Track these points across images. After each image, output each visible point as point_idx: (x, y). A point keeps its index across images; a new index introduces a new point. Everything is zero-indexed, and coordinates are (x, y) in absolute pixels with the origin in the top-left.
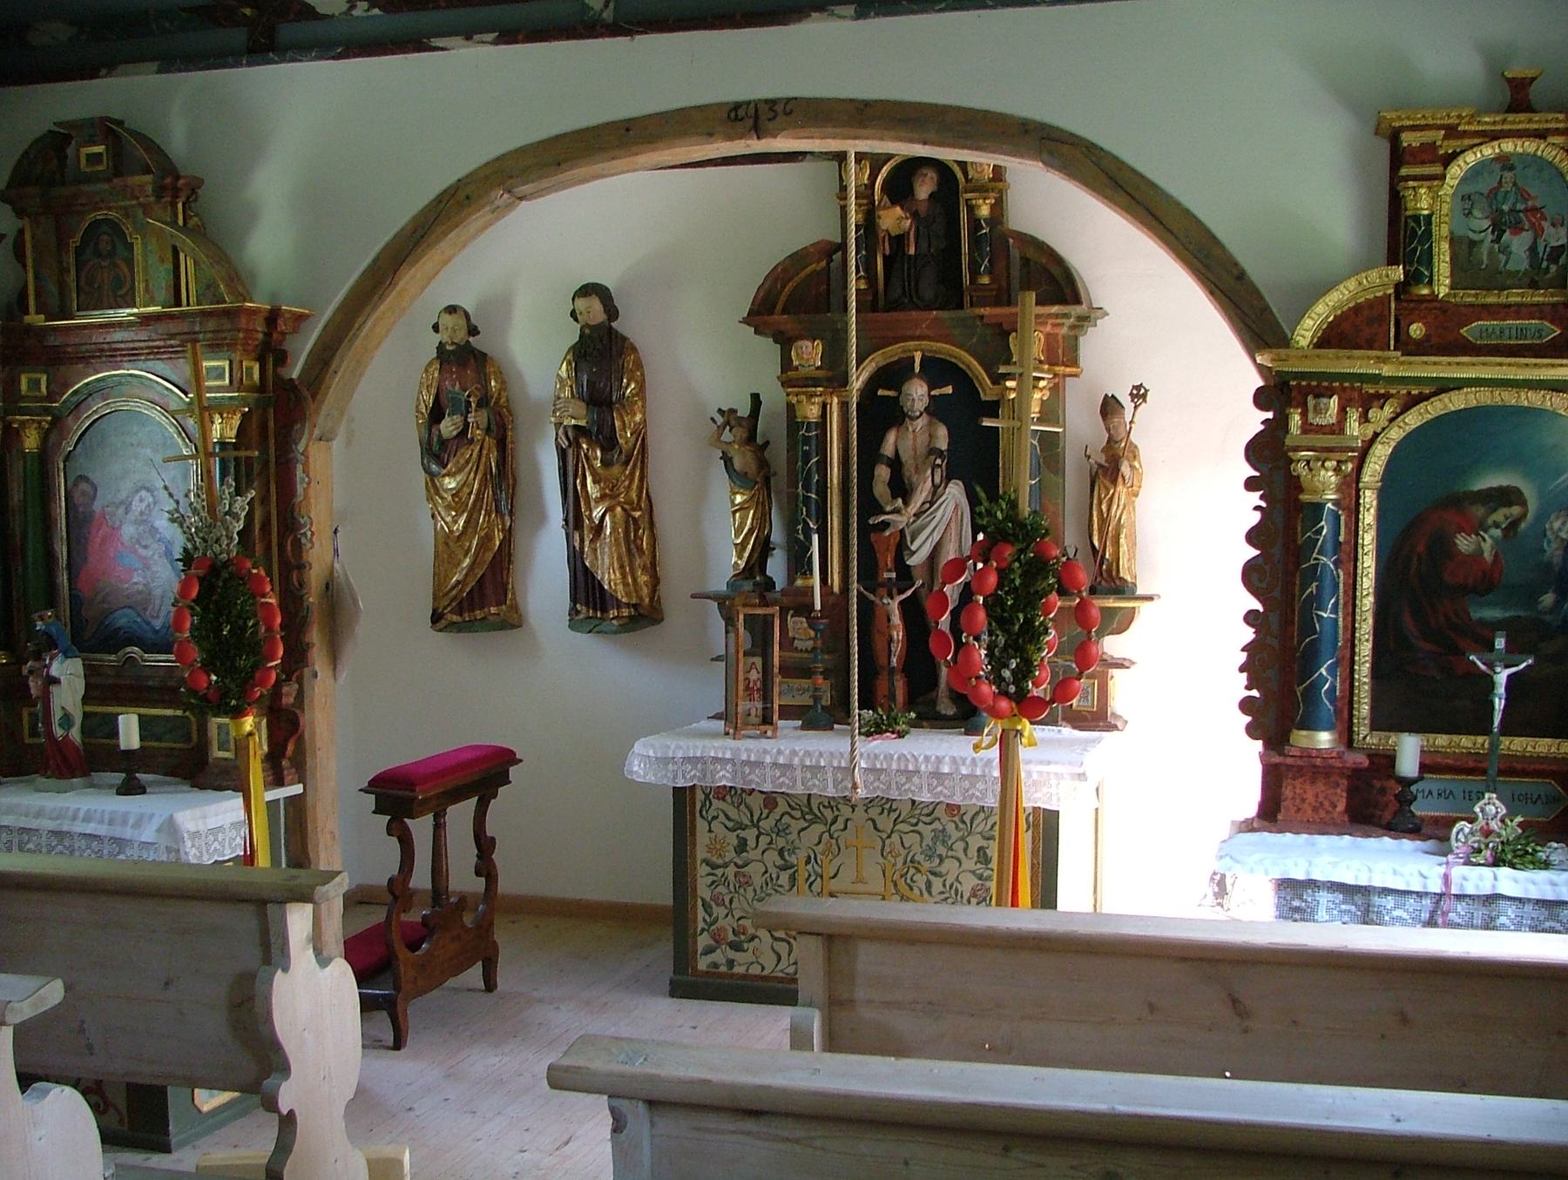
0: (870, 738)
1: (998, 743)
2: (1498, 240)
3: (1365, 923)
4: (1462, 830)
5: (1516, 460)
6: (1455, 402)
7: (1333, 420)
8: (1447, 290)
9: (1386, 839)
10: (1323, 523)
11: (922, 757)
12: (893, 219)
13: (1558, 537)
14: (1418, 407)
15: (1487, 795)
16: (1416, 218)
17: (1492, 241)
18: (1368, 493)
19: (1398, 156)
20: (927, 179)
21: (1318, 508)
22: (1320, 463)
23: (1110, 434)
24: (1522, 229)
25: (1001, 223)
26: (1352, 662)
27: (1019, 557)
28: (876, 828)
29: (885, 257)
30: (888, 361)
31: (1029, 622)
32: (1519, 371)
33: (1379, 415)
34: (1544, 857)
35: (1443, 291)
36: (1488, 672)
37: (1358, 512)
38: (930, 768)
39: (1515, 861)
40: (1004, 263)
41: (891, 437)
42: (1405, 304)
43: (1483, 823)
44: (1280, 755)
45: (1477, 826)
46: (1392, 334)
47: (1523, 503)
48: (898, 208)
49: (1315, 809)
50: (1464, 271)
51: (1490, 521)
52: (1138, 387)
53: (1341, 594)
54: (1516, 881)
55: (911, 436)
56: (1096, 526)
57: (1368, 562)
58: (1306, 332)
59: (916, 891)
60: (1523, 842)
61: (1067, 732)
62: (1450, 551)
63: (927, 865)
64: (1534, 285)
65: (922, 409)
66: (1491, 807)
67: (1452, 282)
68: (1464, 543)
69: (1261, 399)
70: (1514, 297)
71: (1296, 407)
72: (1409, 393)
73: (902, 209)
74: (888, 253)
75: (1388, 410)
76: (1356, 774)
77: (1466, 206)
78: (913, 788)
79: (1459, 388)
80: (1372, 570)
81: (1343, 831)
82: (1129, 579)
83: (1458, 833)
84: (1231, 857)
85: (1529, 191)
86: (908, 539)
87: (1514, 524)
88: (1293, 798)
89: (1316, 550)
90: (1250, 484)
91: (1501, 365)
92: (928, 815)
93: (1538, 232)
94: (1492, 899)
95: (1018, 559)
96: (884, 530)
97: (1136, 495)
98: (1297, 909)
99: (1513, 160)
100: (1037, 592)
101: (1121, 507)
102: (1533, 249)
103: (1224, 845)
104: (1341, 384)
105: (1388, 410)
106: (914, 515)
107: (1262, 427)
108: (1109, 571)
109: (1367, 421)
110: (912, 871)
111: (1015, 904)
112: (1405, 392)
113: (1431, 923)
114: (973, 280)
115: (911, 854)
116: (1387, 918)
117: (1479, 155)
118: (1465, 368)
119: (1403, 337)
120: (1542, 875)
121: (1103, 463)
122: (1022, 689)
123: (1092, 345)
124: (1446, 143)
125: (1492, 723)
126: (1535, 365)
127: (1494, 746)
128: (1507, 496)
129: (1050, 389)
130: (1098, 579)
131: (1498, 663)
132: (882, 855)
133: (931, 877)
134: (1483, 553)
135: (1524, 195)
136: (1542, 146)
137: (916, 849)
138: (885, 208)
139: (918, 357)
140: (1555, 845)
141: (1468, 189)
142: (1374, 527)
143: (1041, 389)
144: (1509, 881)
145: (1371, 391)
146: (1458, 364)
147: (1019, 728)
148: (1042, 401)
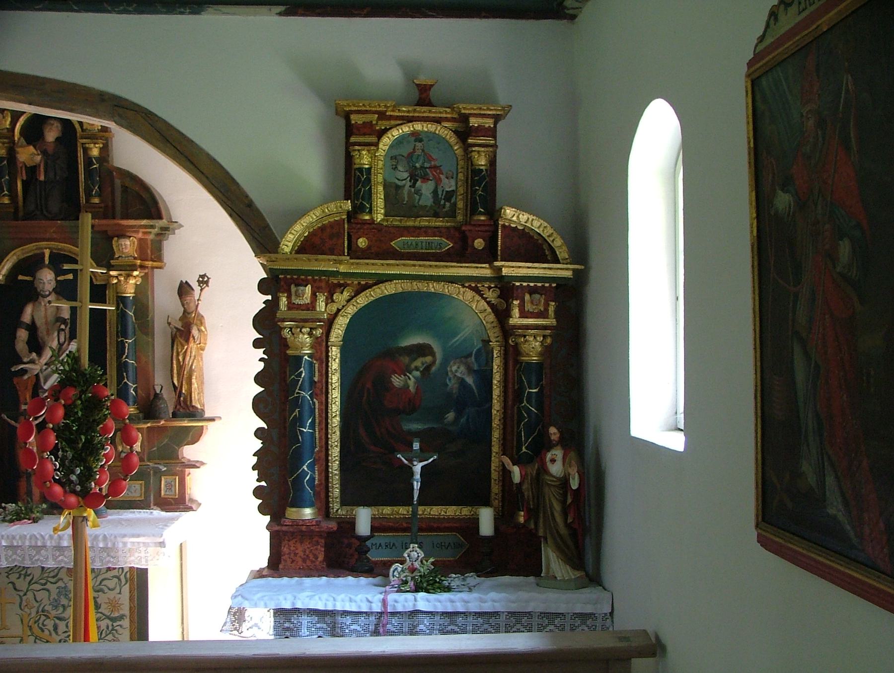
0: (12, 524)
1: (71, 526)
2: (413, 186)
3: (334, 635)
4: (396, 569)
5: (427, 326)
6: (389, 289)
7: (308, 301)
8: (382, 217)
9: (350, 578)
10: (302, 369)
11: (48, 535)
12: (27, 155)
13: (455, 375)
14: (365, 292)
15: (411, 546)
16: (360, 170)
17: (410, 186)
18: (334, 349)
19: (350, 130)
20: (54, 128)
21: (299, 358)
22: (299, 329)
23: (184, 308)
24: (428, 179)
25: (107, 162)
26: (327, 461)
27: (81, 396)
28: (15, 589)
29: (23, 181)
30: (25, 256)
31: (89, 442)
32: (427, 270)
33: (341, 298)
34: (447, 584)
35: (379, 217)
36: (409, 465)
37: (327, 361)
38: (54, 544)
39: (429, 587)
40: (110, 189)
41: (29, 309)
42: (354, 226)
43: (410, 564)
44: (278, 525)
45: (406, 566)
46: (346, 246)
47: (433, 354)
48: (31, 147)
49: (304, 561)
50: (393, 204)
51: (413, 366)
52: (203, 276)
53: (317, 416)
54: (428, 601)
55: (43, 309)
56: (175, 371)
57: (335, 395)
58: (288, 243)
59: (47, 632)
60: (433, 575)
61: (157, 513)
62: (389, 386)
63: (54, 613)
64: (436, 215)
65: (51, 290)
66: (414, 553)
67: (386, 212)
68: (397, 381)
69: (263, 287)
70: (424, 222)
71: (283, 292)
72: (359, 283)
73: (35, 147)
74: (25, 178)
75: (346, 295)
76: (330, 534)
77: (394, 163)
78: (41, 558)
79: (391, 281)
80: (338, 400)
81: (323, 574)
82: (199, 407)
83: (394, 572)
84: (242, 597)
85: (432, 155)
86: (42, 380)
87: (428, 368)
88: (289, 554)
89: (298, 387)
90: (257, 344)
91: (414, 265)
92: (54, 577)
93: (438, 181)
94: (415, 613)
95: (80, 398)
96: (23, 375)
97: (203, 349)
98: (288, 629)
99: (423, 136)
100: (94, 421)
101: (192, 358)
102: (435, 192)
103: (241, 588)
104: (313, 278)
105: (346, 295)
106: (45, 364)
107: (264, 305)
108: (185, 401)
109: (333, 301)
110: (43, 618)
111: (86, 639)
112: (356, 282)
113: (376, 633)
114: (87, 201)
115: (42, 606)
116: (347, 631)
117: (401, 131)
118: (407, 268)
119: (353, 248)
120: (445, 596)
121: (180, 327)
122: (87, 488)
123: (172, 248)
124: (380, 122)
125: (413, 498)
126: (436, 266)
127: (415, 513)
128: (423, 350)
129: (141, 277)
130: (178, 407)
131: (415, 459)
132: (20, 606)
133: (57, 621)
134: (409, 387)
135: (429, 158)
136: (439, 128)
137: (46, 601)
138: (21, 147)
139: (47, 253)
140: (454, 575)
141: (395, 152)
142: (339, 371)
143: (135, 277)
144: (424, 601)
145: (335, 282)
146: (387, 264)
147: (85, 515)
148: (136, 285)
